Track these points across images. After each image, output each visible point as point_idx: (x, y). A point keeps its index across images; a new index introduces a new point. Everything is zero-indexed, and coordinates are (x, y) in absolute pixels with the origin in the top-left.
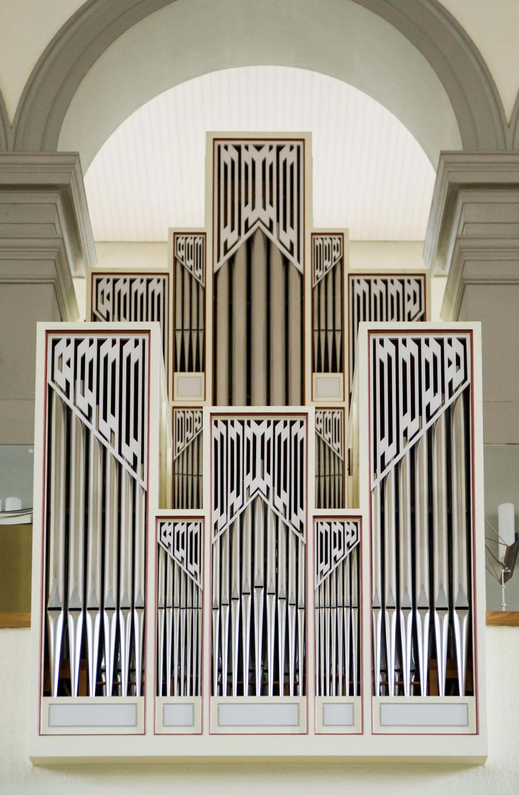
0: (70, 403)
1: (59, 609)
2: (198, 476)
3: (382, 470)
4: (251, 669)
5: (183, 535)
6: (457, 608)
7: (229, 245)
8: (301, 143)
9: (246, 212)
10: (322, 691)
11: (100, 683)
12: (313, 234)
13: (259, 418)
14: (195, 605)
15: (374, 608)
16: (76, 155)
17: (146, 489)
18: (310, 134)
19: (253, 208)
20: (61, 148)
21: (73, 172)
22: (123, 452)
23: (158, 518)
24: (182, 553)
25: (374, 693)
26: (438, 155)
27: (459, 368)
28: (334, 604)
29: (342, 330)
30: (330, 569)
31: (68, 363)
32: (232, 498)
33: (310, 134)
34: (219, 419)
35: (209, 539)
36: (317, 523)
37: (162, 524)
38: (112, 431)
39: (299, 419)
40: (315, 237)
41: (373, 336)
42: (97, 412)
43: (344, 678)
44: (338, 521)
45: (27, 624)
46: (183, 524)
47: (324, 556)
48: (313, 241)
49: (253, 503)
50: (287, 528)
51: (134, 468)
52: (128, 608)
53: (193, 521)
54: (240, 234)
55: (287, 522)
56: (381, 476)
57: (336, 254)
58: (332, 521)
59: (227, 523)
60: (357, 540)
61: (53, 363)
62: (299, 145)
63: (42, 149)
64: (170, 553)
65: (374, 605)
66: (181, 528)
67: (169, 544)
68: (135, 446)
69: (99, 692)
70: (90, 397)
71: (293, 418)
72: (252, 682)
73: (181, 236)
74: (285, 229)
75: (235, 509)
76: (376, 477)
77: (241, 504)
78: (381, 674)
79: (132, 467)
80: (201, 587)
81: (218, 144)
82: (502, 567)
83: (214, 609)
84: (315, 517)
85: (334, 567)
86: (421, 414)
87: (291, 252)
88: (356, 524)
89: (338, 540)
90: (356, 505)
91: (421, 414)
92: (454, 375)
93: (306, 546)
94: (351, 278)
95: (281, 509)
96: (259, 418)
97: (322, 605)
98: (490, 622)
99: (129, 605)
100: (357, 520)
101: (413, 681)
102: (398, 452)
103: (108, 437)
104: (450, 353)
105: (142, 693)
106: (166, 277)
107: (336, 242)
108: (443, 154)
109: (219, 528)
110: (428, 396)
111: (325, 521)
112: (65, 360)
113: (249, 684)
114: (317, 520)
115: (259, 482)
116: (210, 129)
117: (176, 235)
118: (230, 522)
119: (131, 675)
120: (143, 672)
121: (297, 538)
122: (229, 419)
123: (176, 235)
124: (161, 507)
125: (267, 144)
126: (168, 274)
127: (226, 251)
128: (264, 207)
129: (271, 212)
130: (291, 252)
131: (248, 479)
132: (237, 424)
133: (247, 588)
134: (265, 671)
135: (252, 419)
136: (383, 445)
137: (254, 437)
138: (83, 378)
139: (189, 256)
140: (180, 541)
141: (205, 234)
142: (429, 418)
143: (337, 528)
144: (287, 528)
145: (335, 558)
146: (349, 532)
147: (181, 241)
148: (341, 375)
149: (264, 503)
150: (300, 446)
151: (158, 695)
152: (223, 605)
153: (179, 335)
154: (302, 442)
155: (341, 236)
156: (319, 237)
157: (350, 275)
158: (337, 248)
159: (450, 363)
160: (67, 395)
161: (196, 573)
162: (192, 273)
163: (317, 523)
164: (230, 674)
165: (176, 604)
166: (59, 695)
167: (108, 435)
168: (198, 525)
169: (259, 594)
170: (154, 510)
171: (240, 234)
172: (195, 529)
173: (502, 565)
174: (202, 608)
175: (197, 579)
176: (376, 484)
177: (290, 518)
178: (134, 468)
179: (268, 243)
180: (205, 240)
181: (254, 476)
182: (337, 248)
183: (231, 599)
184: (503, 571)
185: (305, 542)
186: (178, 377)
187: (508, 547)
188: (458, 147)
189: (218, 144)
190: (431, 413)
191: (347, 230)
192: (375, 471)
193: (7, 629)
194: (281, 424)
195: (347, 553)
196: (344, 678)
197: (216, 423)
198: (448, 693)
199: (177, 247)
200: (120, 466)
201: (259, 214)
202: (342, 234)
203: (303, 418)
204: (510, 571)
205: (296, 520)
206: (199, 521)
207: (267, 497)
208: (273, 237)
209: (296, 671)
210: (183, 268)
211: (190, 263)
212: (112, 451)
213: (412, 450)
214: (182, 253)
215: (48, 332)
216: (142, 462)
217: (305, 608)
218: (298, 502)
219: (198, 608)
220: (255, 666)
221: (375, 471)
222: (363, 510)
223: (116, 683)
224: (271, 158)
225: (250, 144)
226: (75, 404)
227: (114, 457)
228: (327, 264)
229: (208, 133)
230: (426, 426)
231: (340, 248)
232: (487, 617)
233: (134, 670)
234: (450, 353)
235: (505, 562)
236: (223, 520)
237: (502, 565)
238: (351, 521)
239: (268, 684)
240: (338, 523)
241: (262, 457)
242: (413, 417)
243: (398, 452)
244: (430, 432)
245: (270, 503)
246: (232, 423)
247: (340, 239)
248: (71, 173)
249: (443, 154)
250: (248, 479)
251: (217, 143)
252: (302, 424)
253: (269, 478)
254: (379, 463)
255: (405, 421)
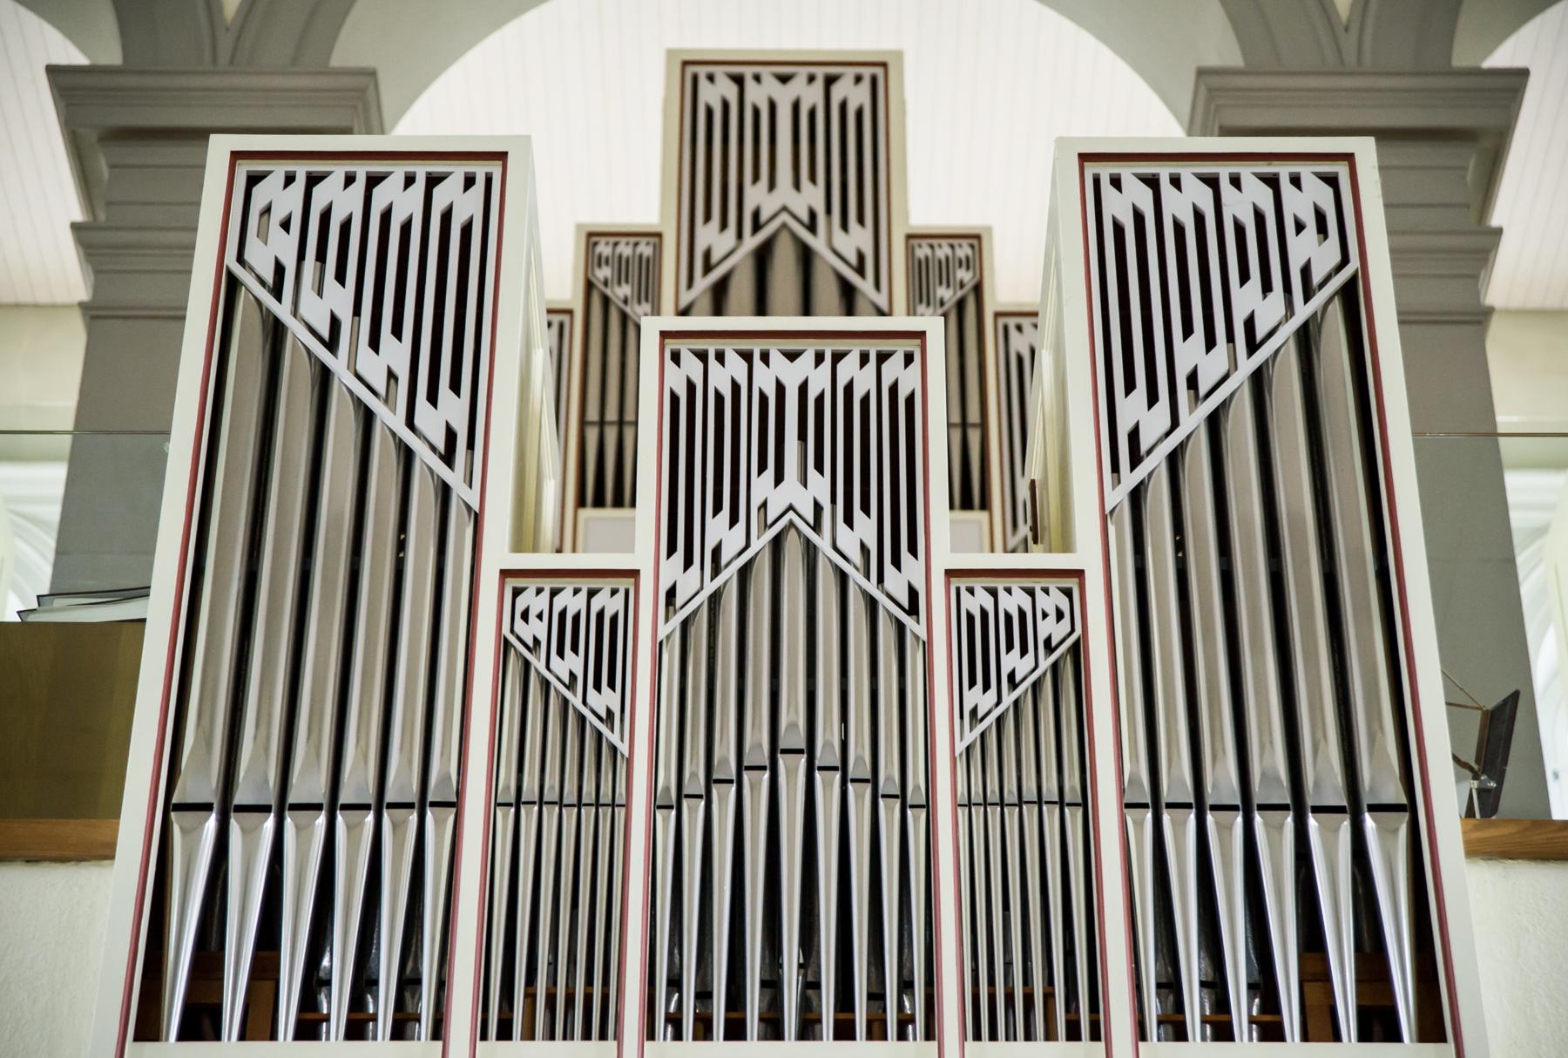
0: (282, 311)
1: (207, 807)
2: (621, 423)
3: (1133, 466)
4: (767, 977)
5: (576, 618)
6: (1374, 808)
7: (715, 258)
8: (879, 71)
9: (756, 195)
10: (981, 1026)
11: (309, 1016)
12: (909, 237)
13: (792, 345)
14: (606, 797)
15: (1128, 806)
16: (372, 74)
17: (476, 507)
18: (899, 55)
19: (772, 185)
20: (337, 61)
21: (360, 106)
22: (417, 422)
23: (505, 574)
24: (573, 662)
25: (1142, 1035)
26: (1192, 77)
27: (1326, 237)
28: (1011, 795)
29: (984, 425)
30: (998, 704)
31: (286, 225)
32: (717, 528)
33: (899, 55)
34: (685, 347)
35: (650, 628)
36: (958, 590)
37: (517, 592)
38: (391, 376)
39: (900, 347)
40: (915, 242)
41: (1091, 169)
42: (354, 332)
43: (1049, 996)
44: (1016, 584)
45: (104, 852)
46: (576, 591)
47: (977, 667)
48: (910, 251)
49: (777, 544)
50: (872, 604)
51: (448, 458)
52: (410, 806)
53: (606, 585)
54: (740, 235)
55: (872, 587)
56: (1130, 479)
57: (963, 275)
58: (1000, 584)
59: (702, 588)
60: (1073, 630)
61: (244, 222)
62: (877, 74)
63: (295, 61)
64: (538, 664)
65: (1128, 799)
66: (570, 602)
67: (536, 641)
68: (453, 408)
69: (308, 1029)
70: (339, 298)
71: (885, 345)
72: (771, 1015)
73: (603, 240)
74: (845, 226)
75: (725, 557)
76: (1117, 481)
77: (743, 544)
78: (1158, 995)
79: (442, 457)
80: (623, 748)
81: (692, 72)
82: (1470, 775)
83: (660, 807)
84: (950, 573)
85: (1008, 699)
86: (1230, 338)
87: (860, 270)
88: (1068, 593)
89: (1019, 631)
90: (1066, 546)
91: (1230, 338)
92: (1311, 251)
93: (927, 648)
94: (1001, 321)
95: (856, 556)
96: (792, 345)
97: (977, 796)
98: (1476, 850)
99: (413, 795)
100: (1072, 583)
101: (1254, 1013)
102: (1175, 423)
103: (381, 387)
104: (1298, 204)
105: (438, 1032)
106: (566, 318)
107: (964, 251)
108: (1202, 73)
109: (679, 603)
110: (1246, 298)
111: (978, 584)
112: (277, 216)
113: (761, 1019)
114: (955, 582)
115: (794, 493)
116: (675, 45)
117: (593, 237)
118: (710, 587)
119: (408, 995)
120: (442, 985)
121: (901, 628)
122: (711, 347)
123: (593, 237)
124: (518, 546)
125: (803, 72)
126: (570, 312)
127: (708, 268)
128: (797, 185)
129: (813, 196)
130: (860, 270)
131: (762, 486)
132: (732, 358)
133: (758, 750)
134: (811, 985)
135: (774, 348)
136: (1132, 408)
137: (780, 389)
138: (321, 256)
139: (622, 275)
140: (566, 632)
141: (659, 235)
142: (1253, 346)
143: (1013, 602)
144: (872, 604)
145: (1012, 675)
146: (1048, 610)
147: (604, 249)
148: (982, 516)
149: (808, 541)
150: (904, 412)
151: (484, 1037)
152: (688, 796)
153: (592, 435)
154: (910, 400)
155: (975, 242)
156: (924, 242)
157: (997, 315)
158: (967, 263)
159: (1300, 227)
160: (277, 292)
161: (610, 713)
162: (628, 310)
163: (958, 590)
164: (704, 995)
165: (551, 794)
166: (182, 1037)
167: (380, 384)
168: (621, 596)
169: (792, 772)
170: (498, 554)
171: (740, 235)
172: (614, 605)
173: (1471, 769)
174: (627, 806)
175: (612, 731)
176: (1118, 497)
177: (881, 580)
178: (448, 458)
179: (806, 256)
180: (658, 249)
181: (779, 478)
182: (967, 263)
183: (709, 781)
184: (1475, 784)
185: (924, 636)
186: (587, 520)
187: (1485, 713)
188: (1234, 59)
189: (692, 72)
190: (1259, 335)
191: (989, 229)
192: (1115, 468)
193: (46, 864)
194: (852, 360)
195: (1045, 663)
196: (1049, 996)
197: (676, 357)
198: (1365, 1035)
199: (592, 258)
200: (407, 455)
201: (784, 199)
202: (978, 237)
203: (912, 346)
204: (1493, 784)
205: (896, 583)
206: (623, 584)
207: (817, 527)
208: (817, 243)
209: (906, 985)
210: (606, 301)
211: (624, 290)
212: (390, 418)
213: (1215, 422)
214: (604, 272)
215: (236, 156)
216: (471, 445)
217: (928, 806)
218: (903, 536)
219: (613, 805)
220: (781, 966)
221: (1115, 468)
222: (1086, 554)
223: (361, 1016)
224: (812, 96)
225: (765, 72)
226: (295, 313)
227: (394, 434)
228: (946, 294)
229: (670, 53)
230: (1247, 366)
231: (975, 262)
232: (1465, 833)
233: (417, 981)
234: (1298, 204)
235: (1478, 761)
236: (689, 583)
237: (1471, 769)
238: (1053, 584)
239: (820, 1021)
240: (1016, 590)
241: (802, 436)
242: (1210, 343)
243: (1175, 423)
244: (1259, 380)
245: (823, 543)
246: (720, 357)
247: (972, 246)
248: (355, 107)
249: (1202, 73)
250: (762, 486)
251: (690, 70)
252: (909, 358)
253: (819, 485)
254: (1125, 449)
255: (1189, 353)
